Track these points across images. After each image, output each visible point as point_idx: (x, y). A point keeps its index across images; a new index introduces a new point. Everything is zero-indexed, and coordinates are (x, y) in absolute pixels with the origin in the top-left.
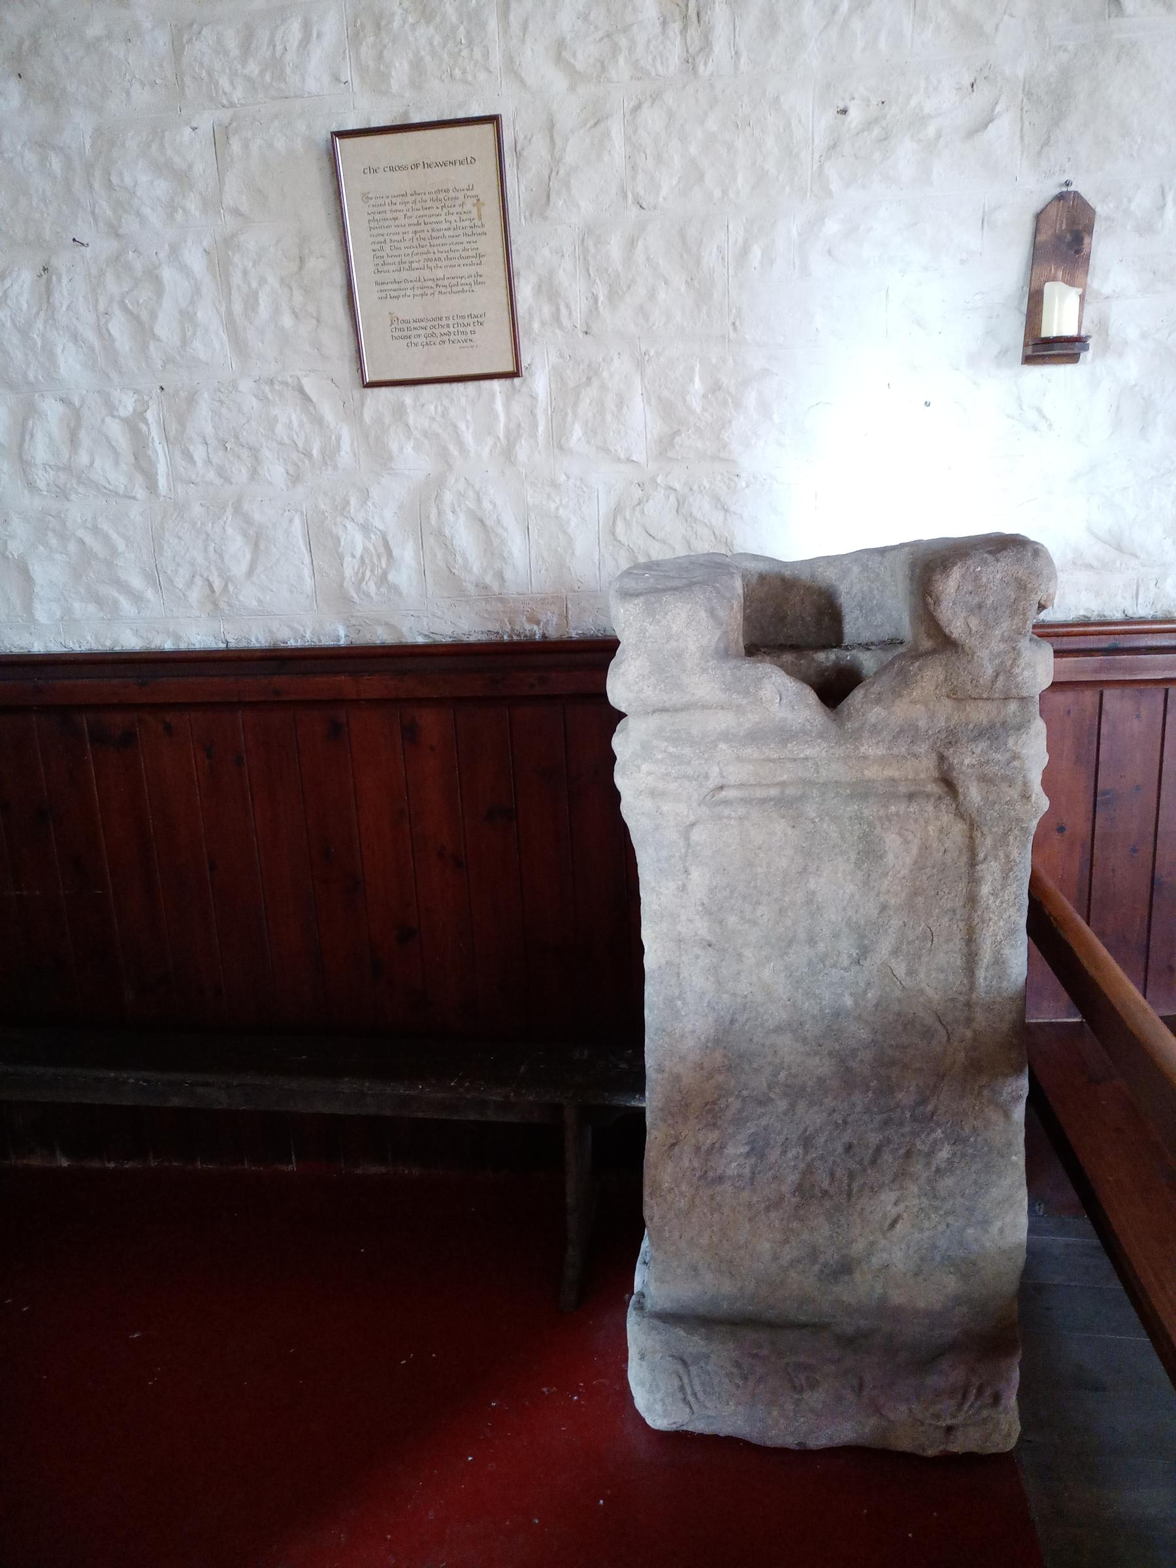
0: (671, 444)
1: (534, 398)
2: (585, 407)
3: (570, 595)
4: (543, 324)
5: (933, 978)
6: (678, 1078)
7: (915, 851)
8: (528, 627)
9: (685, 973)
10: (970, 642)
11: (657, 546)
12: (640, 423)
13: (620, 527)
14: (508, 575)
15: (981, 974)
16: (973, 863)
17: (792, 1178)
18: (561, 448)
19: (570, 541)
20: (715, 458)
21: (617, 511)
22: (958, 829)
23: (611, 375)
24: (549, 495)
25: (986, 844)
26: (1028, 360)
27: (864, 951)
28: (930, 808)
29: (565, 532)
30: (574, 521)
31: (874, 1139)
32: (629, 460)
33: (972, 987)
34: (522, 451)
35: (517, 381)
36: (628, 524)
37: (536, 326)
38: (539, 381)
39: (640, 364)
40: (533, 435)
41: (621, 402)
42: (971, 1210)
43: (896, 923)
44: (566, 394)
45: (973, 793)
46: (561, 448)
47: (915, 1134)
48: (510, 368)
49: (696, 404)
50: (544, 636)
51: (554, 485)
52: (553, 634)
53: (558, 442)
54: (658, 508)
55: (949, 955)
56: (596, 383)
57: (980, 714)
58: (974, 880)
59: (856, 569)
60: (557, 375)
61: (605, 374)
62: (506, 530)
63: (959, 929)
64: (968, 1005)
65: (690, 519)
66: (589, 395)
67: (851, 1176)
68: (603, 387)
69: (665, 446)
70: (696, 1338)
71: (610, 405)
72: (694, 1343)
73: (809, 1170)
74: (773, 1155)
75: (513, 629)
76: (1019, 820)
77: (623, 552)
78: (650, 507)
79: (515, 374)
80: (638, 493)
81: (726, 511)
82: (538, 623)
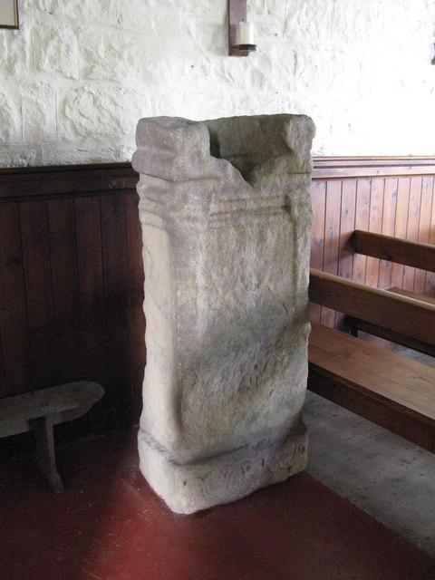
0: (91, 71)
1: (24, 42)
2: (51, 50)
3: (43, 144)
4: (29, 5)
5: (281, 287)
6: (195, 353)
7: (276, 237)
8: (20, 160)
9: (198, 302)
10: (296, 151)
11: (85, 120)
12: (76, 63)
13: (67, 110)
14: (11, 133)
15: (299, 283)
16: (295, 239)
17: (237, 387)
18: (38, 69)
19: (43, 116)
20: (111, 80)
21: (65, 102)
22: (290, 226)
23: (63, 36)
24: (32, 92)
25: (299, 231)
26: (231, 54)
27: (260, 281)
28: (281, 218)
29: (41, 112)
30: (45, 106)
31: (264, 360)
32: (71, 78)
33: (295, 289)
34: (18, 68)
35: (15, 31)
36: (71, 109)
37: (25, 6)
38: (27, 32)
39: (77, 32)
40: (24, 61)
41: (68, 49)
42: (294, 380)
43: (270, 267)
44: (41, 43)
45: (296, 212)
46: (38, 69)
47: (277, 355)
48: (13, 24)
49: (102, 55)
50: (28, 165)
51: (34, 86)
52: (33, 163)
53: (36, 66)
54: (85, 100)
55: (287, 278)
56: (56, 38)
57: (297, 179)
58: (296, 246)
59: (225, 126)
60: (35, 32)
61: (61, 35)
62: (10, 109)
63: (290, 268)
64: (294, 297)
65: (100, 108)
66: (53, 43)
67: (257, 377)
68: (60, 41)
69: (88, 73)
70: (206, 467)
71: (63, 49)
72: (206, 469)
73: (244, 380)
74: (230, 378)
75: (12, 162)
76: (309, 220)
77: (69, 123)
78: (81, 101)
79: (16, 27)
80: (75, 94)
81: (116, 105)
82: (25, 158)
